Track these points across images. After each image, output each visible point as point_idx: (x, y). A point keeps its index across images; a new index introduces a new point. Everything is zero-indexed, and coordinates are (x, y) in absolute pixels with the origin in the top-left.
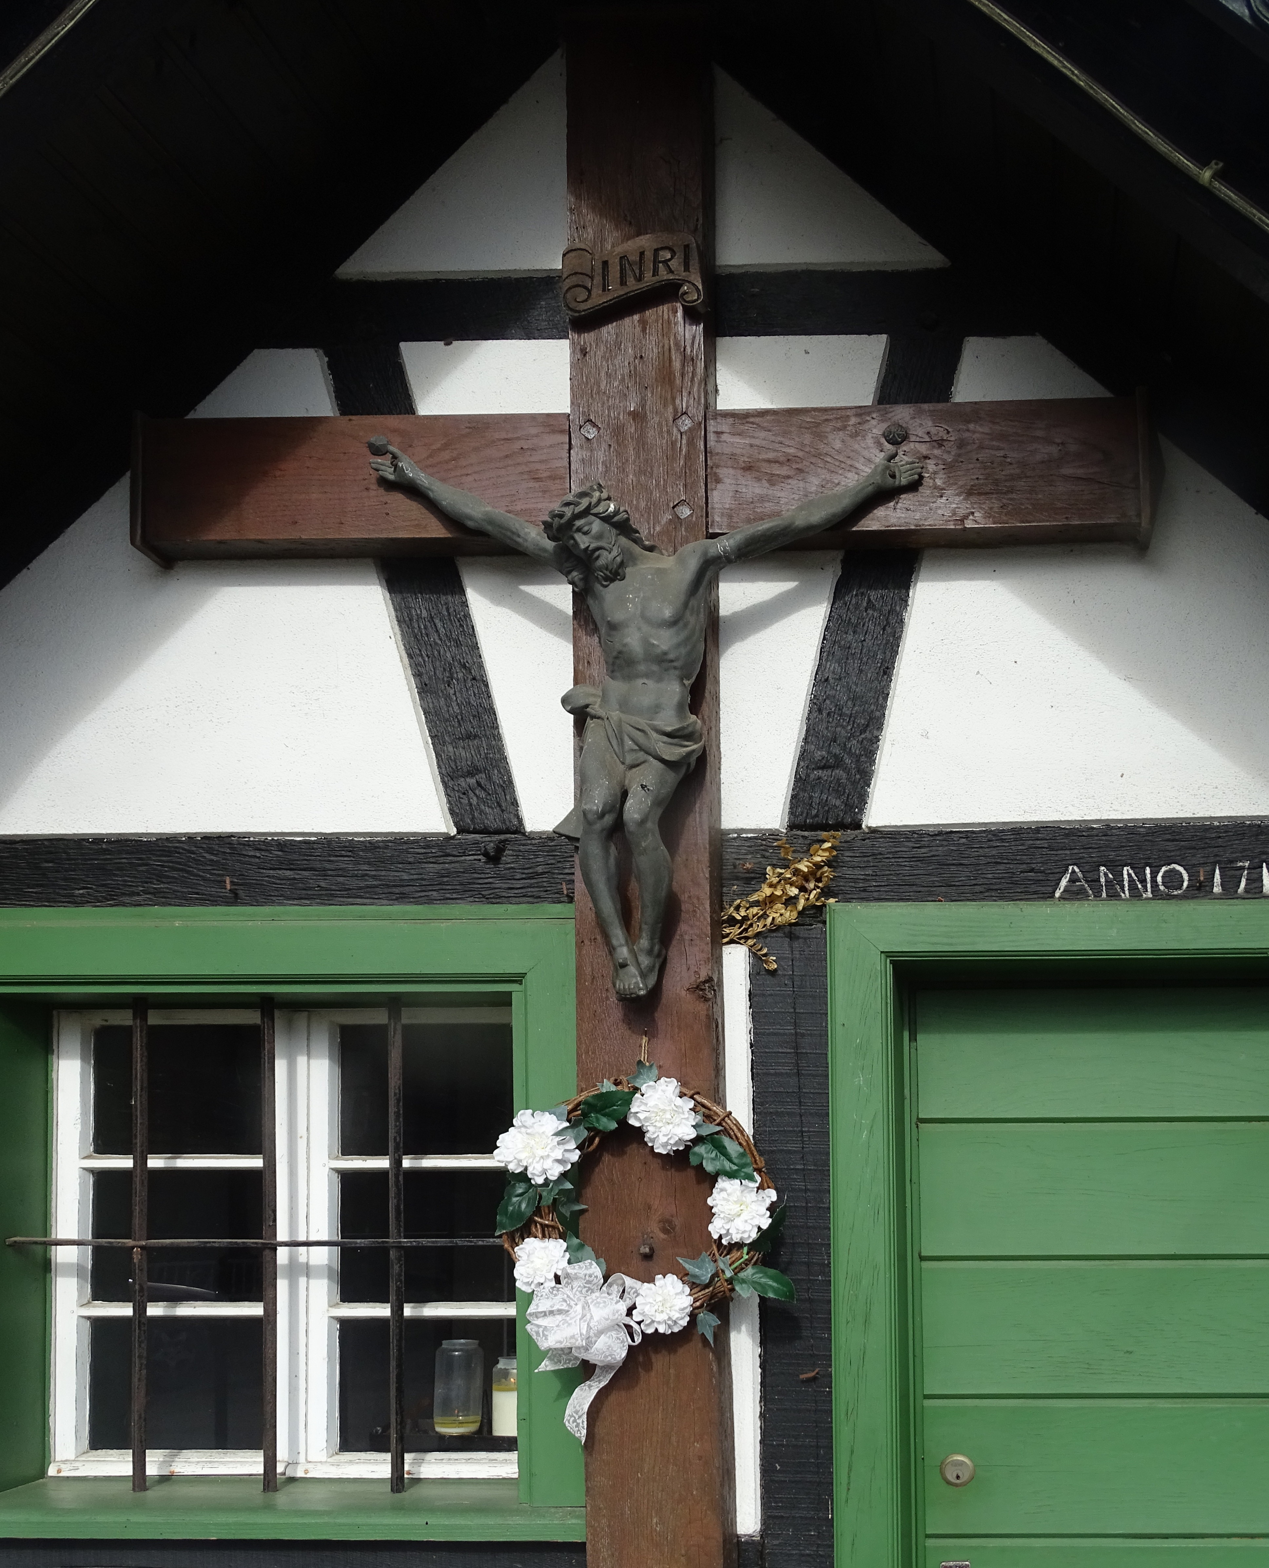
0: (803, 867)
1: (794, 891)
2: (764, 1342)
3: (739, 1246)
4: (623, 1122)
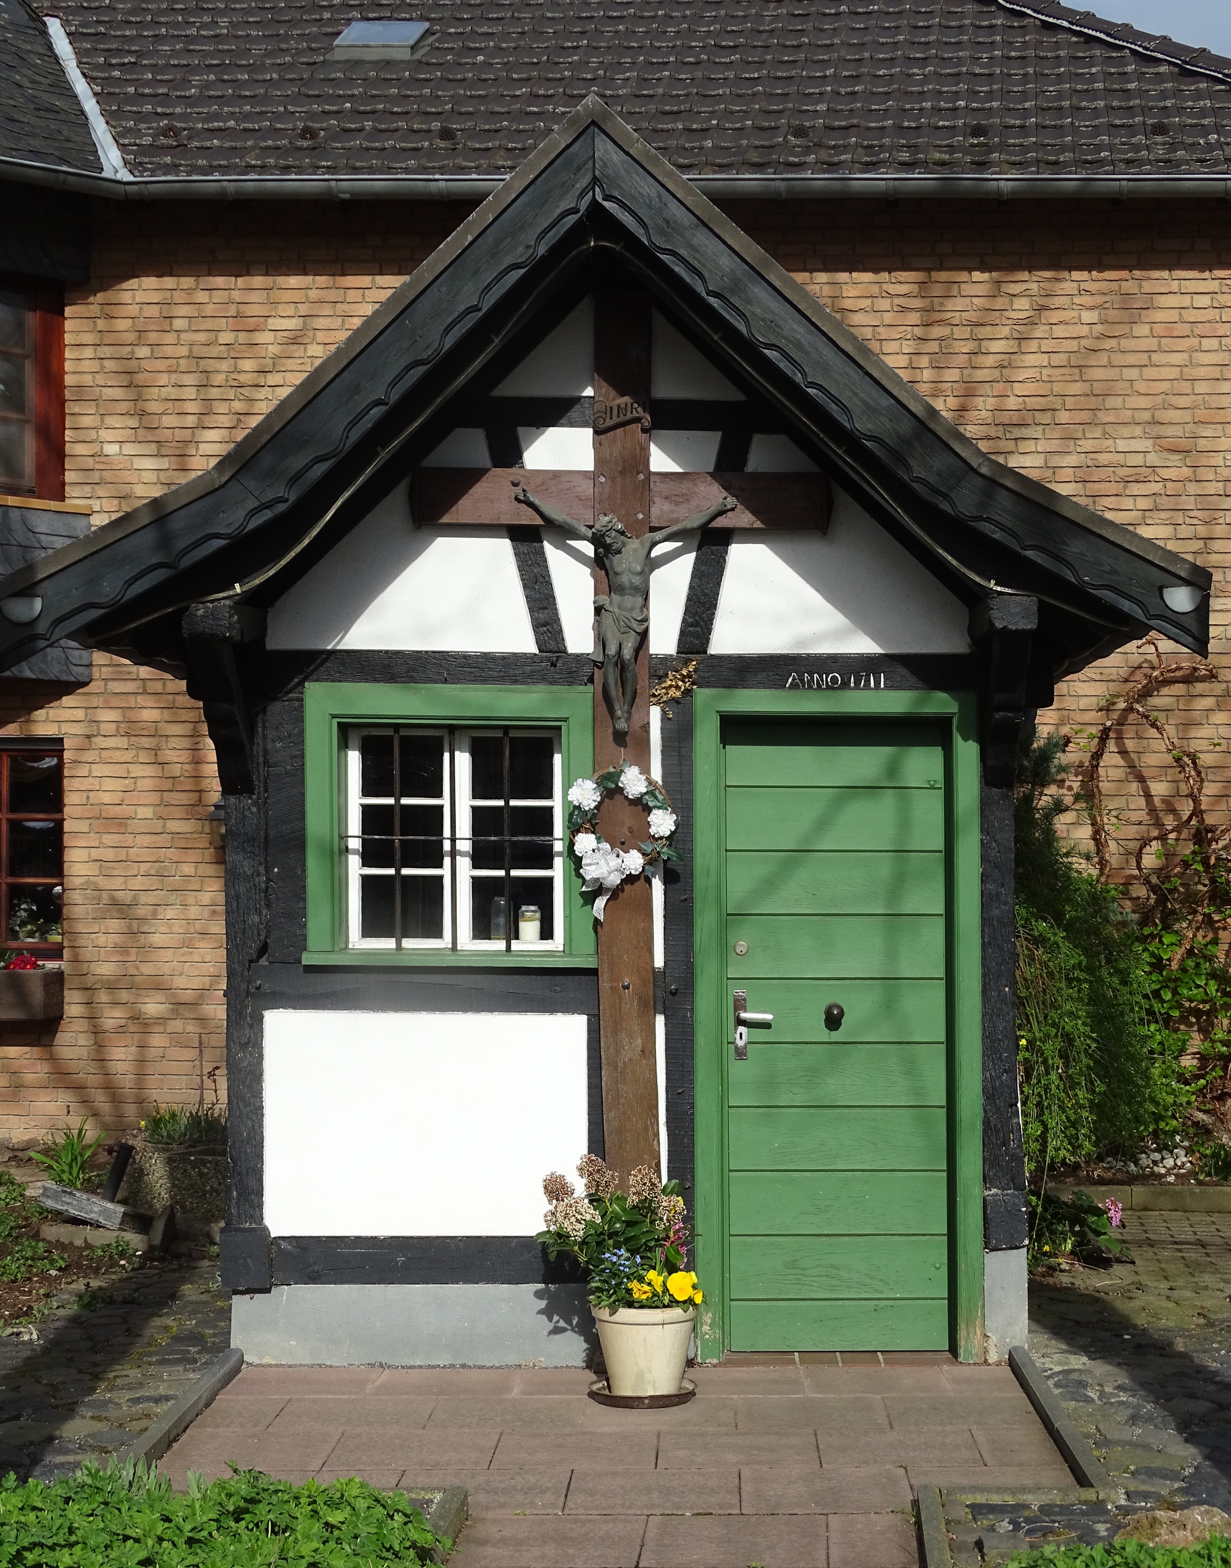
0: (684, 672)
1: (680, 683)
2: (665, 884)
3: (661, 838)
4: (617, 785)
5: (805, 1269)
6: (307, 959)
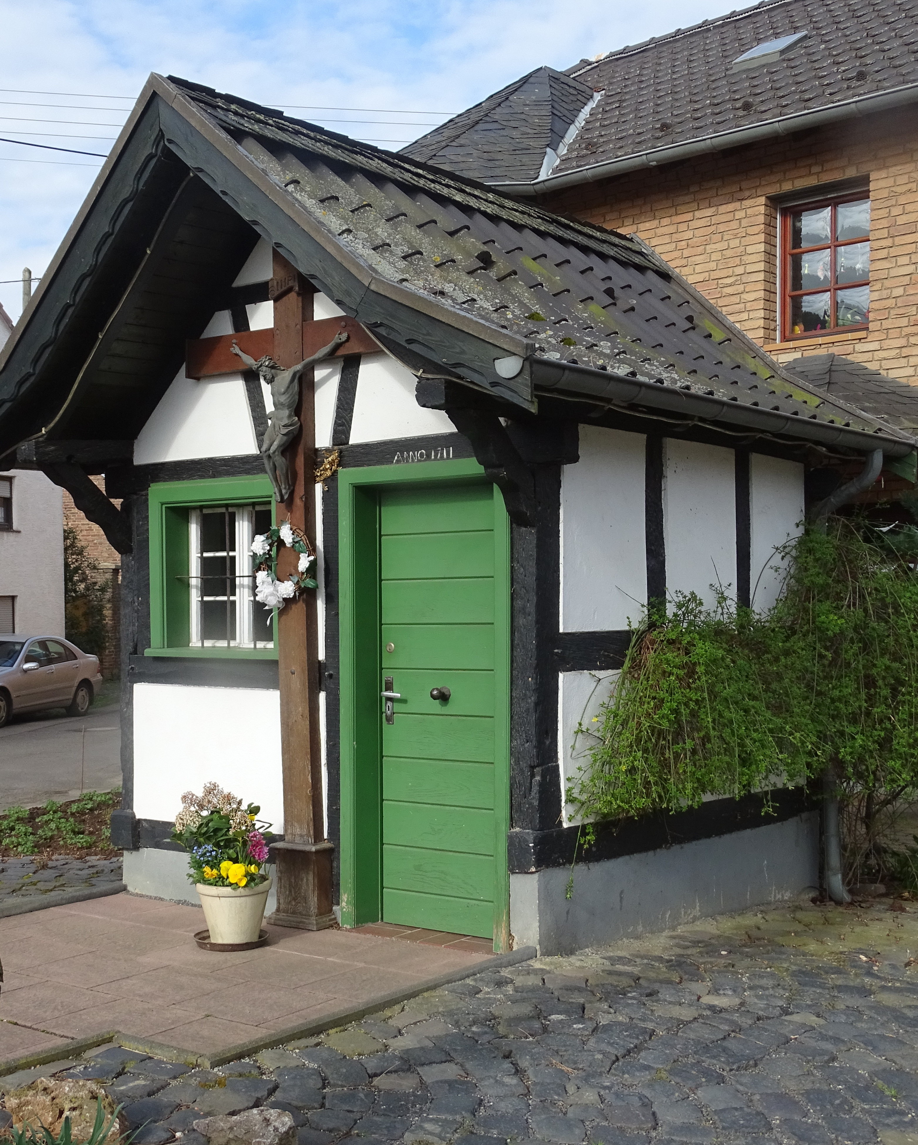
5: (426, 872)
6: (148, 652)
